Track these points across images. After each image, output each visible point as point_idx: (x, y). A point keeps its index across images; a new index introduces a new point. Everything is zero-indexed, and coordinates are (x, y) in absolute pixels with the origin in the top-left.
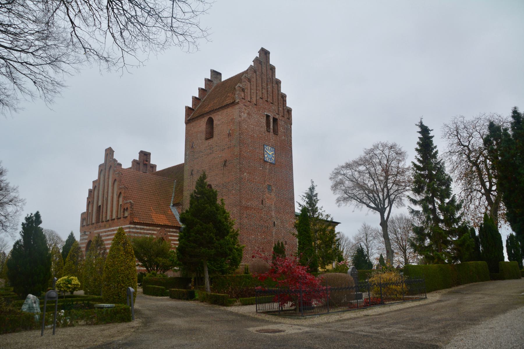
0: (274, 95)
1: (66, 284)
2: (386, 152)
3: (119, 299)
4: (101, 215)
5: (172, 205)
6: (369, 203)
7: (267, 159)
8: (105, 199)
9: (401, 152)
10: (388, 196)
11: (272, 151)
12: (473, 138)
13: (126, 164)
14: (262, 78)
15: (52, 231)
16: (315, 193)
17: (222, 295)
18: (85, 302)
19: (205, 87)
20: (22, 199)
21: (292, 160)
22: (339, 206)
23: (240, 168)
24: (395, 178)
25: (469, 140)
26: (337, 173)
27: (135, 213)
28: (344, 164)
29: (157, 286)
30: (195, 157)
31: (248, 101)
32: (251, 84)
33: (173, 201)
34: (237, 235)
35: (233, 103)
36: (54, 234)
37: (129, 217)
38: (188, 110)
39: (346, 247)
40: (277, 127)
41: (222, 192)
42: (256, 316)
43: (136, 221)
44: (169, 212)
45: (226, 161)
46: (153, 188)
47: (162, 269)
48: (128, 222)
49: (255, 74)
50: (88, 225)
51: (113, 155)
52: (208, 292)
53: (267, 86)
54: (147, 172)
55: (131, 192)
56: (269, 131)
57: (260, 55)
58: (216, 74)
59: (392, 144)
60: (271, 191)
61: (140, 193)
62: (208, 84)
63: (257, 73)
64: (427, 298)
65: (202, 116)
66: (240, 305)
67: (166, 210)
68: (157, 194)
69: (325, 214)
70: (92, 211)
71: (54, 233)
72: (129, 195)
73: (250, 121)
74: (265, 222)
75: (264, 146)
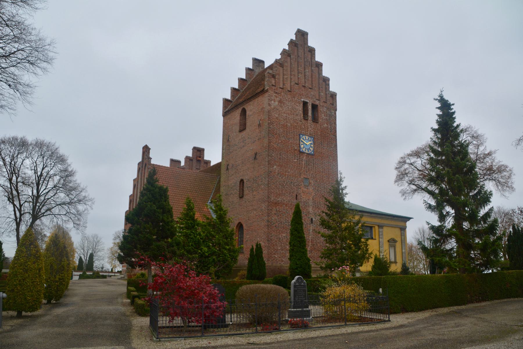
0: (313, 80)
5: (210, 201)
11: (310, 141)
19: (246, 77)
20: (91, 198)
21: (337, 149)
22: (405, 199)
23: (269, 161)
28: (409, 152)
30: (231, 150)
31: (280, 88)
32: (283, 69)
35: (263, 92)
40: (318, 114)
41: (252, 187)
44: (205, 210)
45: (256, 154)
49: (289, 58)
51: (149, 152)
53: (305, 70)
54: (201, 168)
56: (306, 118)
58: (258, 62)
61: (174, 190)
62: (248, 73)
63: (292, 56)
64: (390, 321)
73: (281, 109)
75: (300, 136)
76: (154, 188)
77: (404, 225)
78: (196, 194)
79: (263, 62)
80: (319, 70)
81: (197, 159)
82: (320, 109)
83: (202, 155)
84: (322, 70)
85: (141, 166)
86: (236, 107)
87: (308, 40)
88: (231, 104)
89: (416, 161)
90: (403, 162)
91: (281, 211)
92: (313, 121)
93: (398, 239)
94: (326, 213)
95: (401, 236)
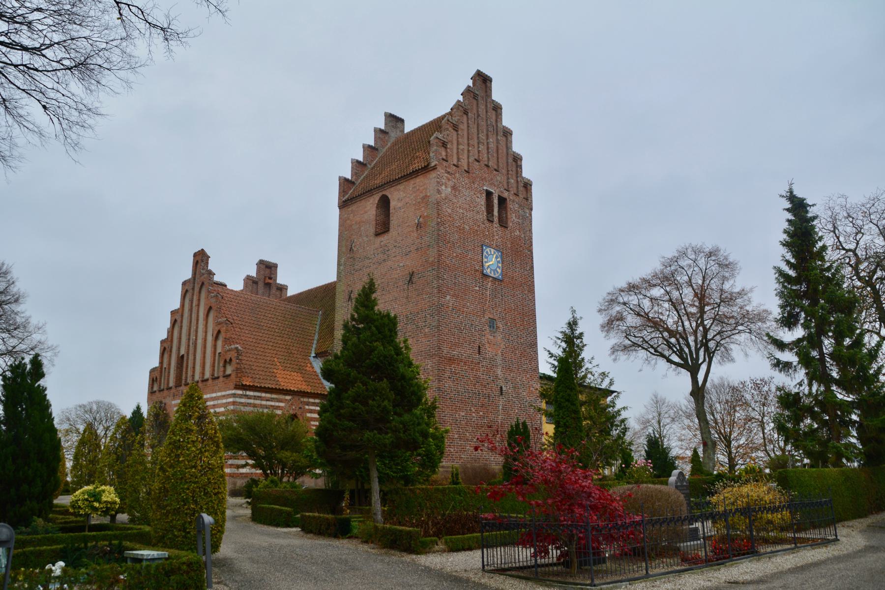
0: (500, 156)
1: (90, 502)
2: (700, 262)
3: (185, 537)
4: (184, 373)
5: (313, 355)
7: (487, 271)
8: (191, 344)
9: (727, 263)
10: (705, 344)
12: (864, 236)
13: (236, 284)
14: (478, 124)
15: (109, 403)
16: (577, 333)
17: (408, 529)
18: (113, 542)
20: (52, 346)
21: (533, 274)
22: (615, 360)
23: (439, 287)
24: (717, 309)
25: (856, 239)
26: (612, 302)
27: (244, 368)
28: (623, 285)
29: (277, 507)
30: (356, 267)
31: (454, 165)
32: (458, 134)
33: (315, 349)
34: (435, 408)
35: (426, 169)
36: (113, 410)
37: (233, 376)
40: (506, 213)
42: (483, 581)
43: (247, 382)
44: (307, 368)
45: (412, 275)
46: (280, 325)
47: (293, 472)
48: (232, 386)
49: (465, 116)
50: (161, 391)
52: (377, 522)
55: (239, 330)
57: (474, 84)
58: (394, 120)
59: (713, 247)
60: (495, 330)
61: (254, 333)
63: (469, 114)
64: (839, 540)
65: (369, 192)
66: (445, 551)
67: (303, 365)
68: (288, 334)
69: (597, 371)
70: (169, 364)
71: (113, 408)
72: (235, 336)
73: (456, 201)
74: (485, 386)
75: (482, 247)
78: (290, 341)
83: (273, 274)
84: (511, 142)
85: (191, 288)
86: (368, 193)
87: (491, 90)
91: (459, 373)
92: (501, 225)
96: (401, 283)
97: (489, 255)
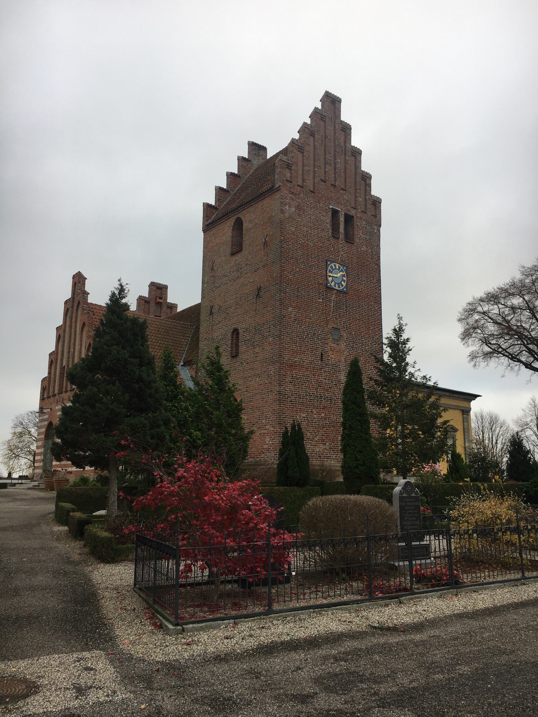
6: (533, 362)
11: (342, 271)
16: (402, 339)
21: (380, 286)
22: (475, 365)
23: (281, 300)
28: (481, 294)
31: (298, 186)
32: (303, 156)
35: (272, 190)
38: (207, 209)
39: (502, 438)
40: (353, 230)
45: (259, 289)
53: (335, 160)
63: (316, 136)
73: (300, 220)
74: (327, 390)
75: (327, 262)
76: (122, 321)
77: (467, 406)
79: (264, 149)
80: (356, 161)
81: (156, 300)
82: (357, 222)
83: (164, 294)
85: (71, 306)
86: (225, 216)
88: (217, 213)
89: (491, 310)
90: (471, 310)
91: (300, 378)
93: (459, 427)
94: (376, 381)
95: (463, 422)
96: (251, 298)
97: (333, 270)
